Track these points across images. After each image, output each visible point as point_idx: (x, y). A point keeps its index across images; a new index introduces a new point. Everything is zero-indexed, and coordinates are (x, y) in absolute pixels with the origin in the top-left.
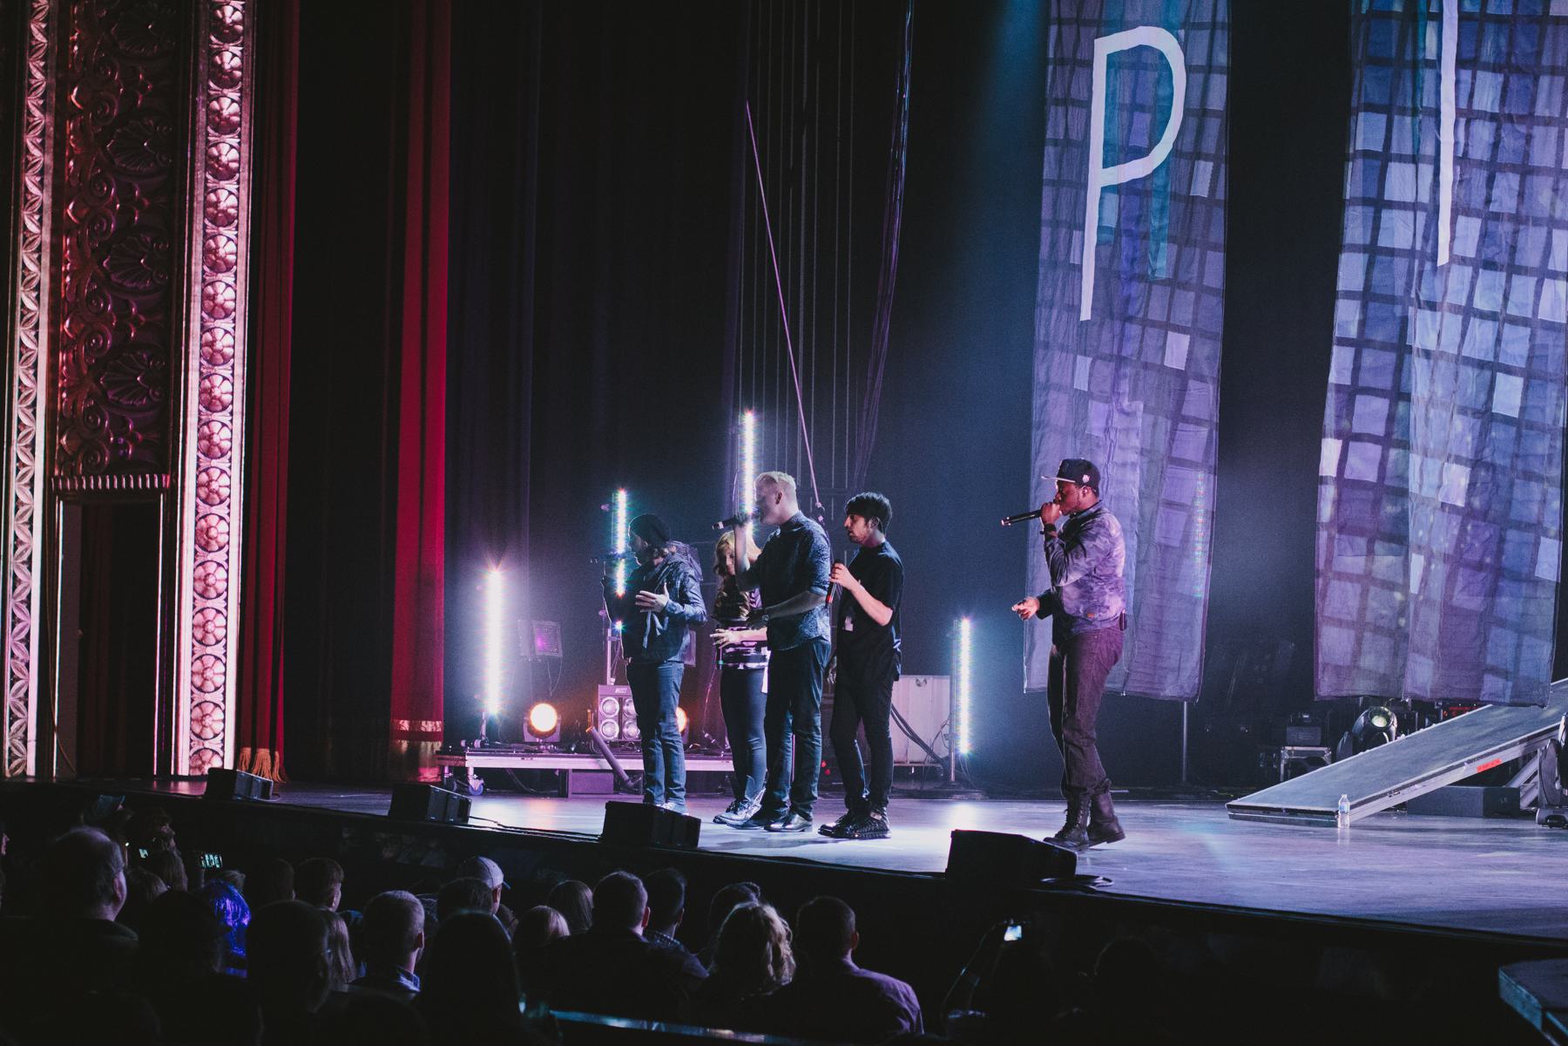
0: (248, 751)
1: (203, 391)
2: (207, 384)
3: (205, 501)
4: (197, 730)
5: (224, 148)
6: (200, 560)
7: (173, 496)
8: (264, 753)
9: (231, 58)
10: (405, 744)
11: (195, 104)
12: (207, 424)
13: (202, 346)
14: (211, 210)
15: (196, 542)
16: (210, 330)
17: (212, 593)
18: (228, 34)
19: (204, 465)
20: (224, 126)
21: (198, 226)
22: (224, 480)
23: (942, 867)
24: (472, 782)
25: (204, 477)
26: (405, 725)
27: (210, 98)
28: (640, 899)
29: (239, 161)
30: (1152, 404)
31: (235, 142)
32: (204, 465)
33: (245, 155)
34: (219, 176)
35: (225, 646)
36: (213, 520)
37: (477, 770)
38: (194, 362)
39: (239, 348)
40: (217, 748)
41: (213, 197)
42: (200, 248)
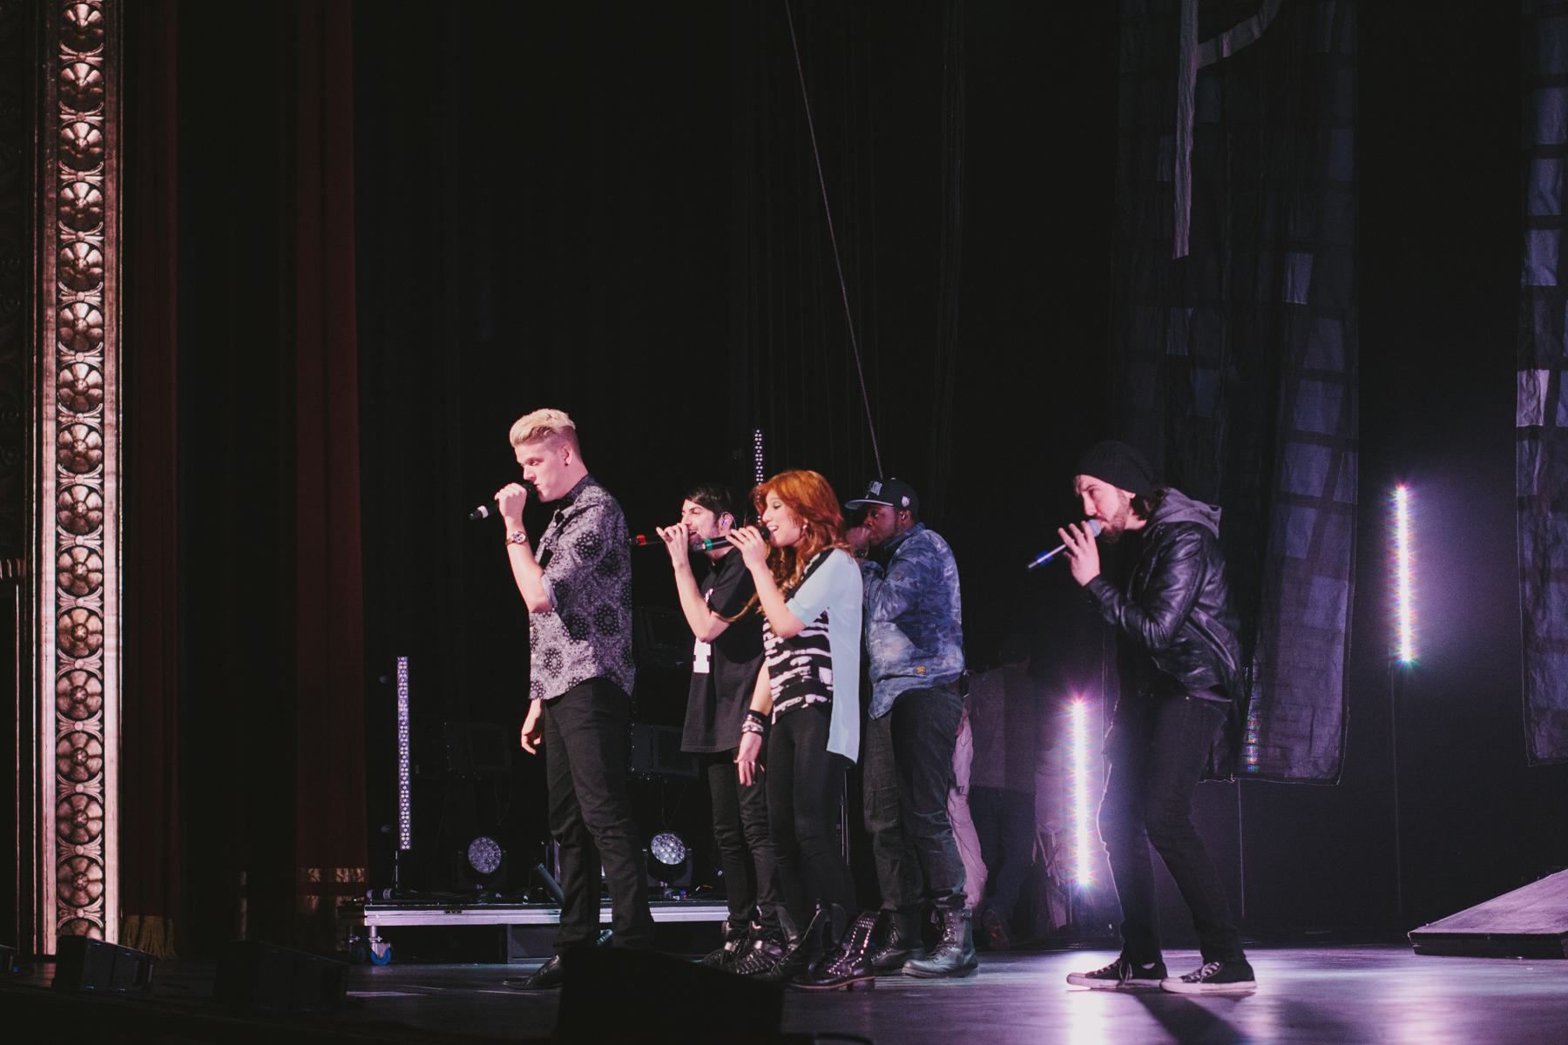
0: (134, 920)
1: (60, 446)
2: (67, 436)
3: (68, 591)
4: (67, 894)
5: (82, 249)
6: (63, 670)
7: (29, 583)
8: (151, 920)
9: (84, 131)
10: (315, 900)
11: (42, 73)
12: (69, 489)
13: (58, 387)
14: (65, 391)
15: (58, 645)
16: (70, 367)
17: (82, 711)
18: (83, 39)
19: (66, 544)
20: (83, 280)
21: (50, 410)
22: (93, 686)
23: (829, 749)
24: (374, 947)
25: (66, 560)
26: (316, 874)
27: (61, 245)
28: (687, 638)
29: (102, 326)
30: (715, 773)
31: (95, 240)
32: (66, 544)
33: (112, 138)
34: (75, 286)
35: (102, 720)
36: (80, 616)
37: (382, 930)
38: (49, 649)
39: (110, 389)
40: (95, 917)
41: (68, 314)
42: (53, 260)
